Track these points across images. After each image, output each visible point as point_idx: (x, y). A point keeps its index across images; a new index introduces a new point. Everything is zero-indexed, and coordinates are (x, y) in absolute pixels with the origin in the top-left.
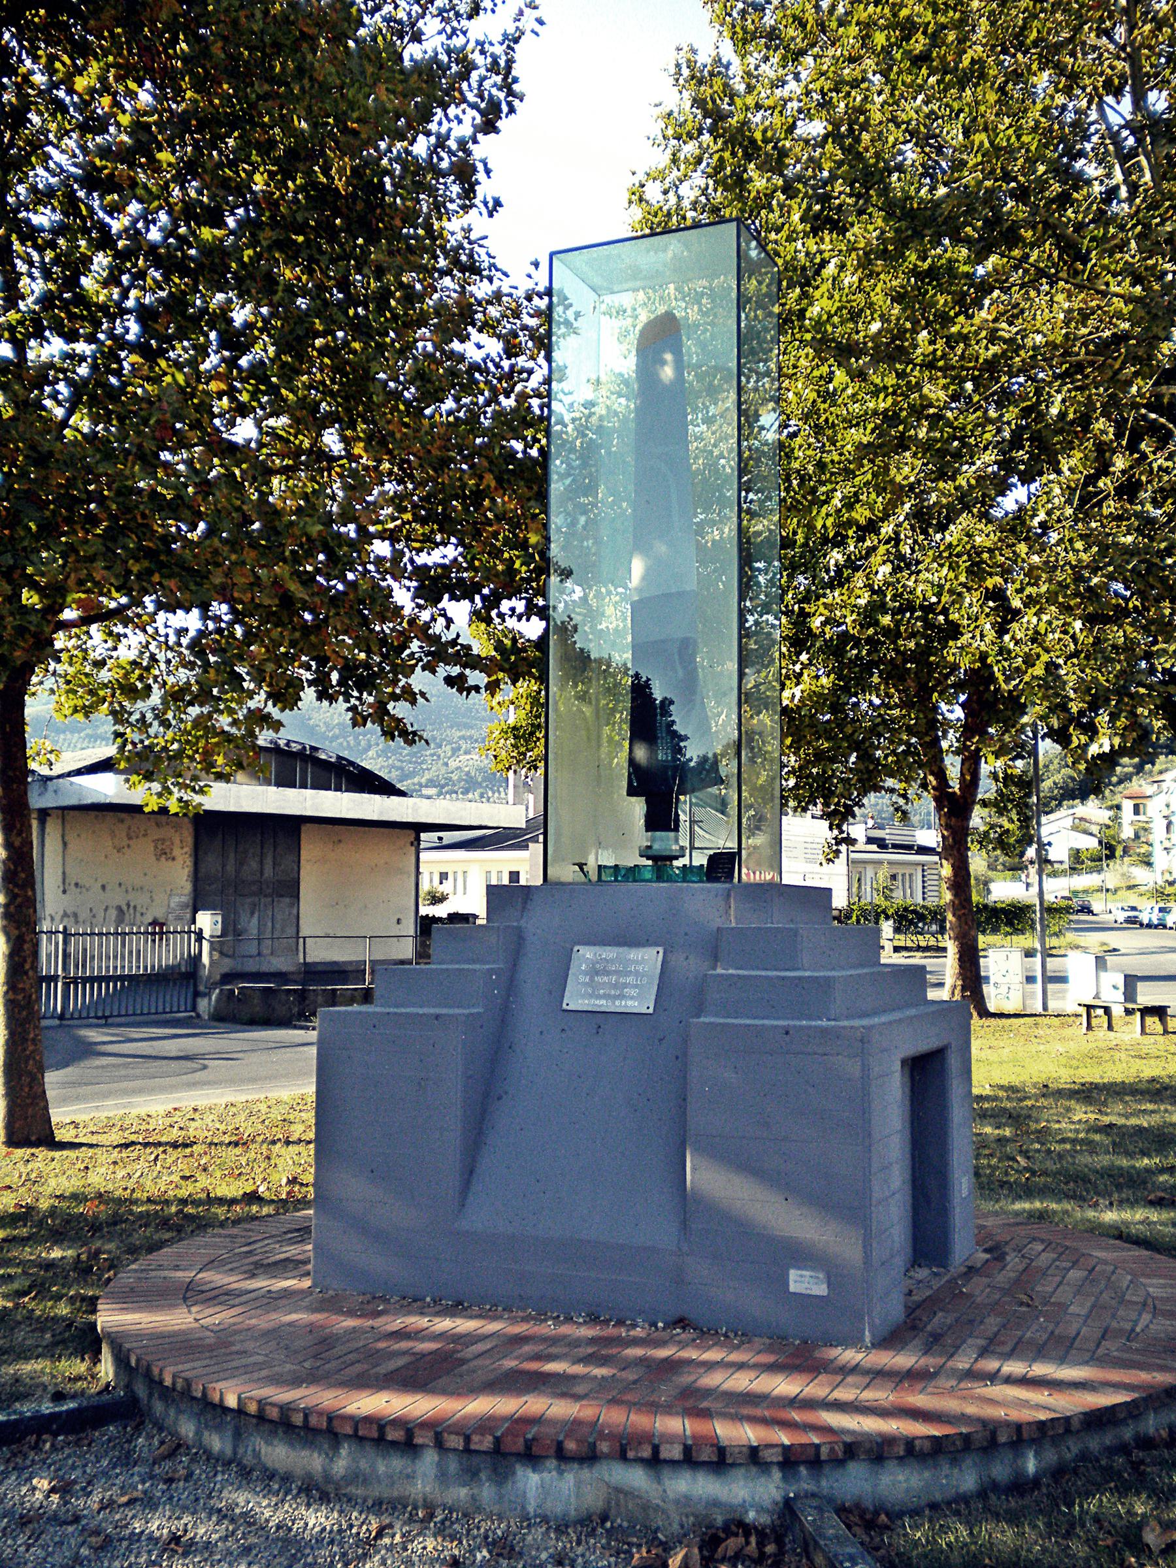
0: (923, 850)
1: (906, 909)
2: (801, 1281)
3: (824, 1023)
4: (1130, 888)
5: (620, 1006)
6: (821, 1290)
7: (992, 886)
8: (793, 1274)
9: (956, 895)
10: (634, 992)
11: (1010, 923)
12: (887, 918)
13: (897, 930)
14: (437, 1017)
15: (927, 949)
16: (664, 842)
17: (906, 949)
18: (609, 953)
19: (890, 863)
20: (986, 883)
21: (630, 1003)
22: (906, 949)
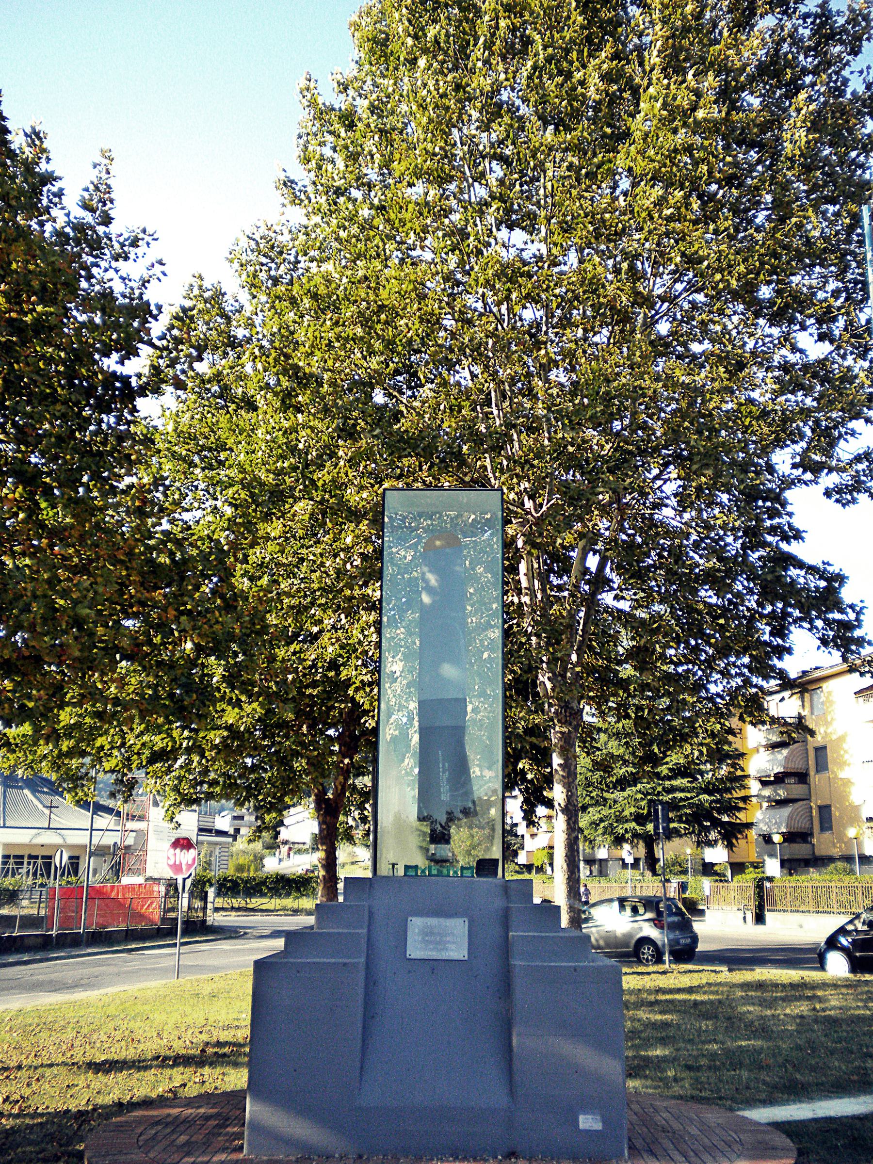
0: (220, 833)
1: (225, 879)
2: (588, 1122)
3: (586, 964)
4: (352, 863)
5: (444, 955)
6: (598, 1126)
7: (265, 861)
8: (581, 1118)
9: (327, 872)
10: (453, 947)
11: (298, 890)
12: (211, 885)
13: (218, 894)
14: (345, 964)
15: (239, 909)
16: (443, 851)
17: (223, 909)
18: (433, 921)
19: (209, 843)
20: (262, 859)
21: (452, 954)
22: (223, 909)
